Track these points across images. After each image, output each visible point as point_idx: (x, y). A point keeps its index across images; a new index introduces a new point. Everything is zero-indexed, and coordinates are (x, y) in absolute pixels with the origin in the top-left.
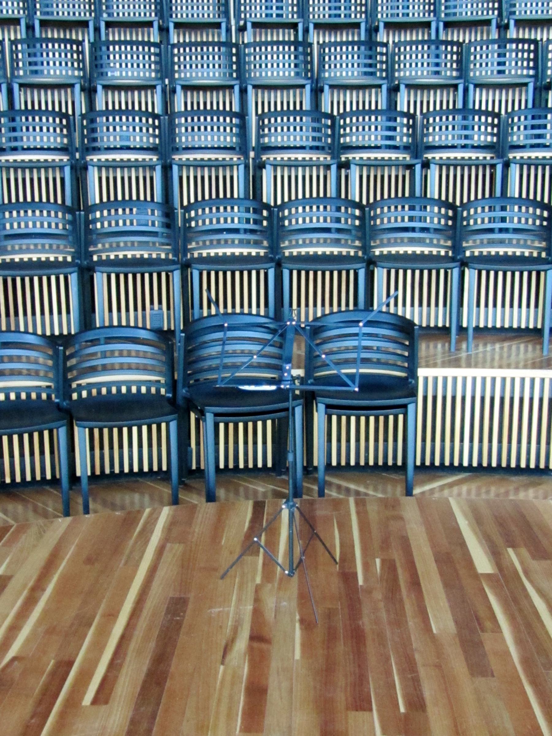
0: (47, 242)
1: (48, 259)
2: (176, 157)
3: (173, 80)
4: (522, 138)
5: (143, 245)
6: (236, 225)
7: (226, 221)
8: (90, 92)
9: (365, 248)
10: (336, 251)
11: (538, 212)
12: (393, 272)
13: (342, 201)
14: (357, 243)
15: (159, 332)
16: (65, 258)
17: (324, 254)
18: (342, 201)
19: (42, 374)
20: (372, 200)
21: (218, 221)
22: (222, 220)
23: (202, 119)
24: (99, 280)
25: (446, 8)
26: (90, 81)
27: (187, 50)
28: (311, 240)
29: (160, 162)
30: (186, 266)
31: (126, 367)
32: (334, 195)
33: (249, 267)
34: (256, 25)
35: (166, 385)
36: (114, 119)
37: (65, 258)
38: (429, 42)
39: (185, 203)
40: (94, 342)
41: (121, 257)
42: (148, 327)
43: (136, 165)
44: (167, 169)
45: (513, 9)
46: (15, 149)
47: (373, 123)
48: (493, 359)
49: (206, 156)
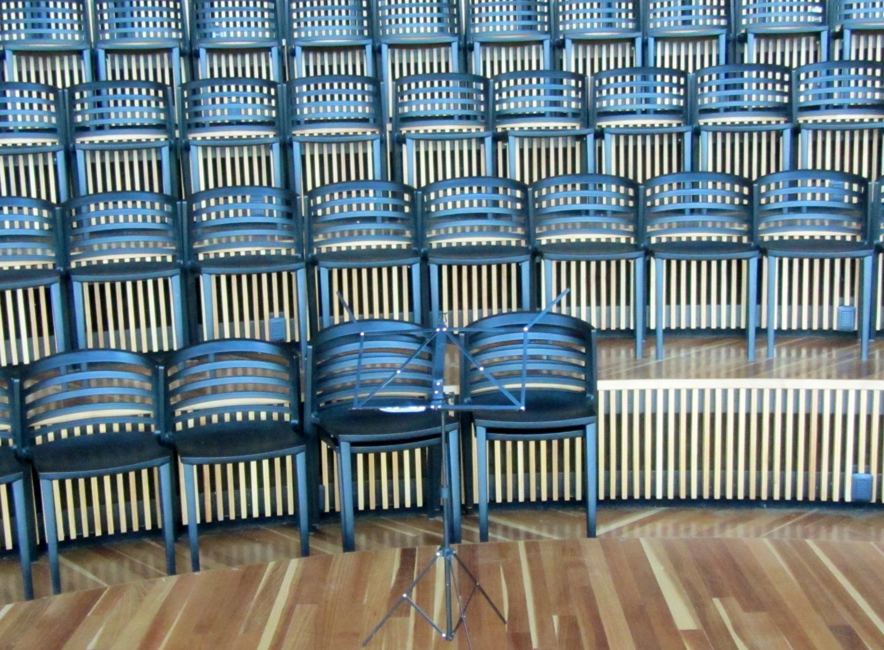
1: (143, 259)
2: (297, 133)
3: (291, 40)
4: (714, 100)
5: (258, 240)
8: (191, 57)
13: (499, 180)
14: (520, 231)
15: (281, 344)
16: (730, 238)
18: (499, 180)
20: (535, 179)
21: (350, 208)
22: (354, 207)
24: (207, 283)
30: (312, 264)
36: (221, 89)
39: (310, 188)
41: (232, 254)
42: (267, 339)
43: (249, 143)
44: (286, 148)
46: (100, 128)
48: (688, 368)
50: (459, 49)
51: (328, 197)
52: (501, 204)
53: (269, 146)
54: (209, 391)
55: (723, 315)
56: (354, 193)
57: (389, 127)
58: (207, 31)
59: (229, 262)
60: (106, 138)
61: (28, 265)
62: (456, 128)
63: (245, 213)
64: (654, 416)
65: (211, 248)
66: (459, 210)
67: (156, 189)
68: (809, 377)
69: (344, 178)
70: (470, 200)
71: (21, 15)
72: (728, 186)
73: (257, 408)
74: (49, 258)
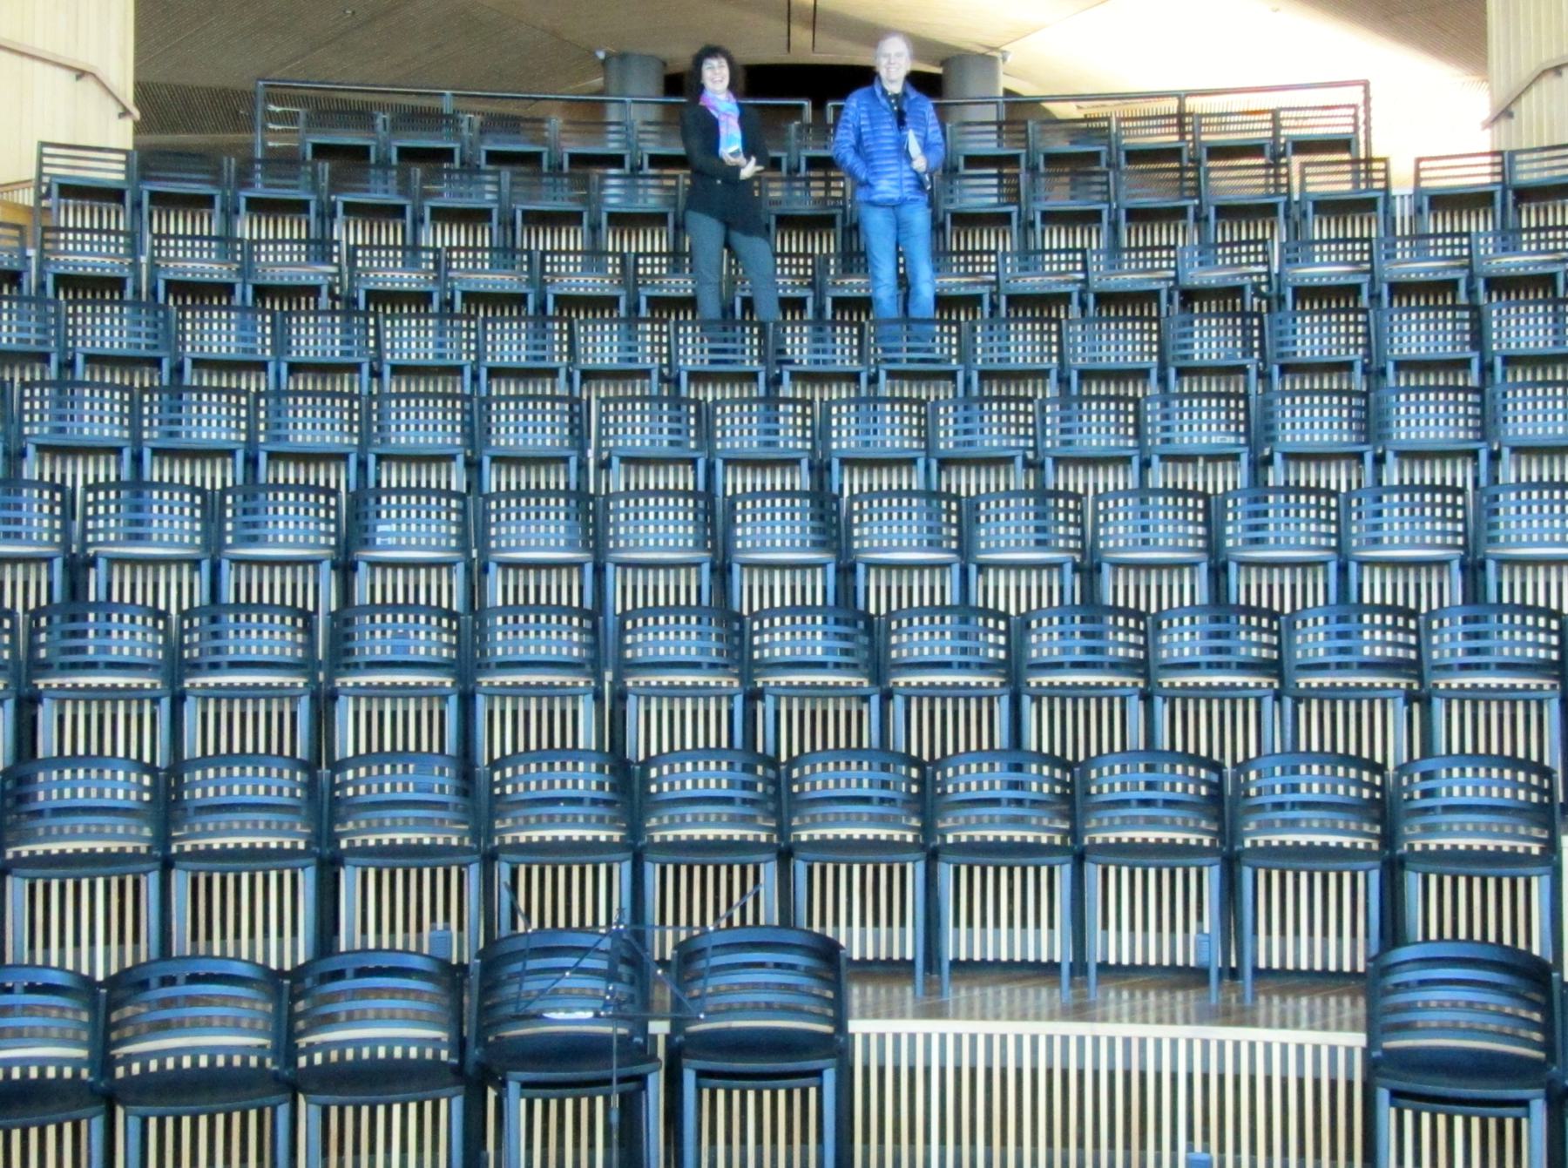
0: (262, 817)
1: (266, 845)
2: (484, 681)
3: (484, 549)
4: (819, 651)
5: (421, 824)
6: (865, 791)
7: (564, 785)
8: (345, 569)
9: (783, 829)
10: (883, 834)
11: (1353, 773)
12: (670, 869)
13: (884, 753)
14: (915, 822)
15: (445, 964)
16: (294, 844)
17: (717, 839)
18: (884, 753)
19: (245, 1024)
20: (938, 755)
21: (551, 785)
22: (557, 784)
23: (532, 618)
24: (348, 879)
26: (348, 552)
27: (513, 503)
28: (979, 818)
29: (1005, 690)
30: (932, 858)
31: (385, 1014)
32: (876, 743)
33: (690, 859)
34: (628, 461)
35: (450, 1045)
36: (384, 619)
37: (294, 844)
38: (858, 401)
40: (338, 975)
41: (386, 842)
42: (426, 951)
43: (417, 692)
44: (467, 702)
46: (215, 666)
48: (984, 1006)
49: (534, 679)
50: (1210, 570)
51: (521, 769)
52: (1303, 788)
53: (444, 698)
54: (343, 1017)
55: (1047, 942)
56: (557, 765)
57: (609, 676)
58: (369, 535)
59: (381, 851)
60: (225, 680)
61: (114, 847)
62: (701, 680)
63: (406, 788)
64: (927, 1071)
65: (355, 834)
66: (701, 791)
67: (287, 752)
68: (1132, 1020)
69: (545, 745)
70: (861, 779)
72: (1507, 774)
73: (406, 1042)
74: (144, 839)
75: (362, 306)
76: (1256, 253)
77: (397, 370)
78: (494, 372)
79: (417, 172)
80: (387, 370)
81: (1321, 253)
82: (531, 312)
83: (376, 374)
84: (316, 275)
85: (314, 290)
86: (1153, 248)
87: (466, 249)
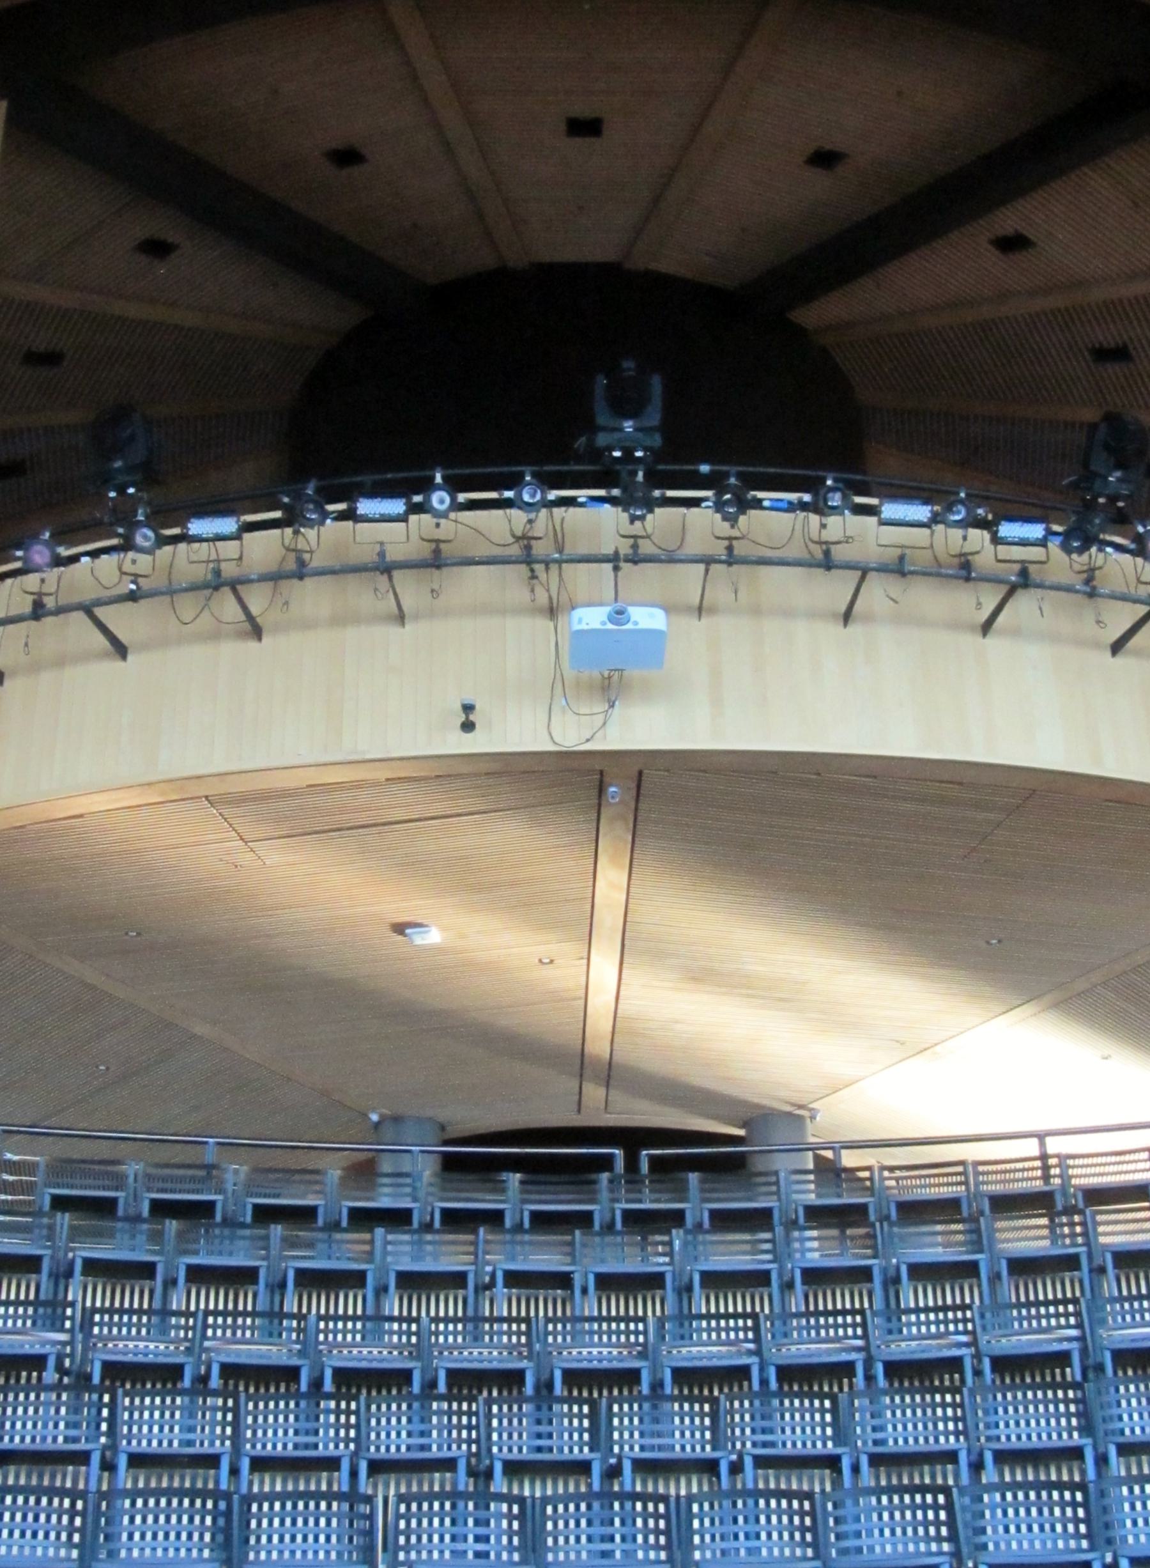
25: (838, 1537)
38: (589, 1497)
45: (983, 1539)
47: (31, 1509)
71: (747, 1417)
75: (96, 1379)
76: (1067, 1315)
77: (138, 1461)
78: (261, 1464)
79: (172, 1226)
80: (123, 1461)
81: (1020, 1319)
82: (304, 1387)
83: (108, 1466)
84: (43, 1344)
85: (37, 1362)
86: (1037, 1304)
87: (225, 1314)
